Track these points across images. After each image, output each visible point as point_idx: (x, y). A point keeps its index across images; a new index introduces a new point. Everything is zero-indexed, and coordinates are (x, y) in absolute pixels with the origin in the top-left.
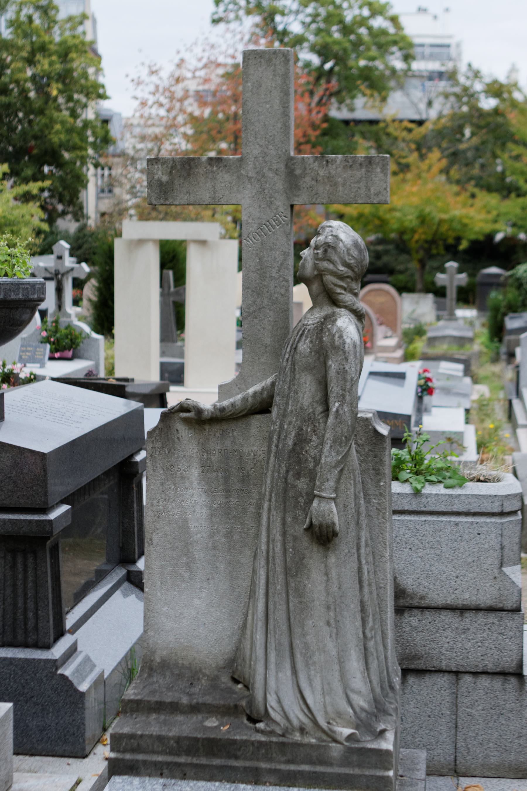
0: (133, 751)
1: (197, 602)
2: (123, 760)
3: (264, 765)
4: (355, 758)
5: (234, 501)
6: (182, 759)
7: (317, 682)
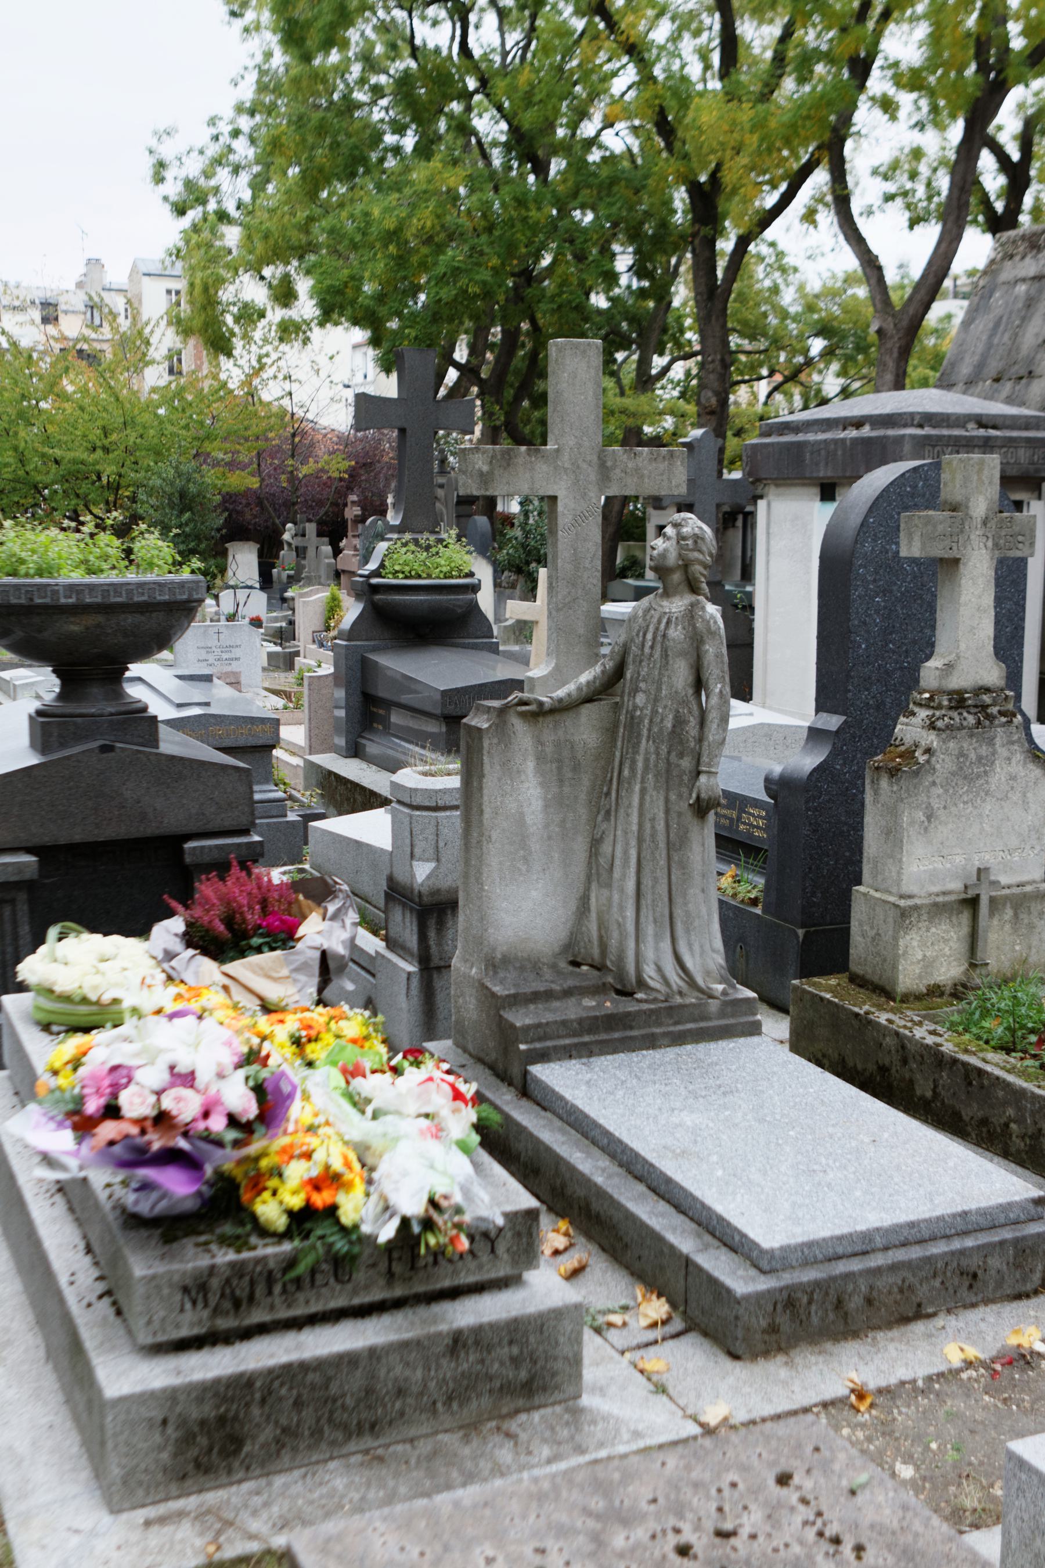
0: (540, 1039)
1: (534, 893)
3: (658, 1030)
4: (729, 1009)
5: (567, 790)
6: (586, 1039)
7: (696, 947)
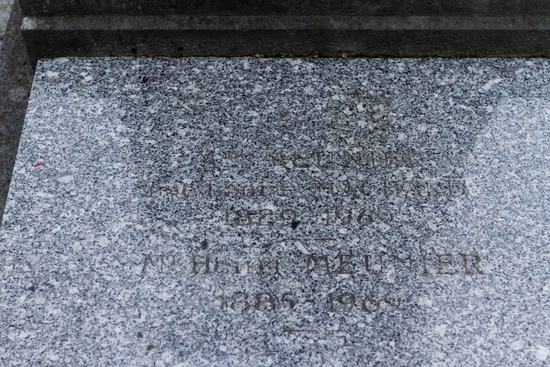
2: (51, 32)
3: (336, 24)
